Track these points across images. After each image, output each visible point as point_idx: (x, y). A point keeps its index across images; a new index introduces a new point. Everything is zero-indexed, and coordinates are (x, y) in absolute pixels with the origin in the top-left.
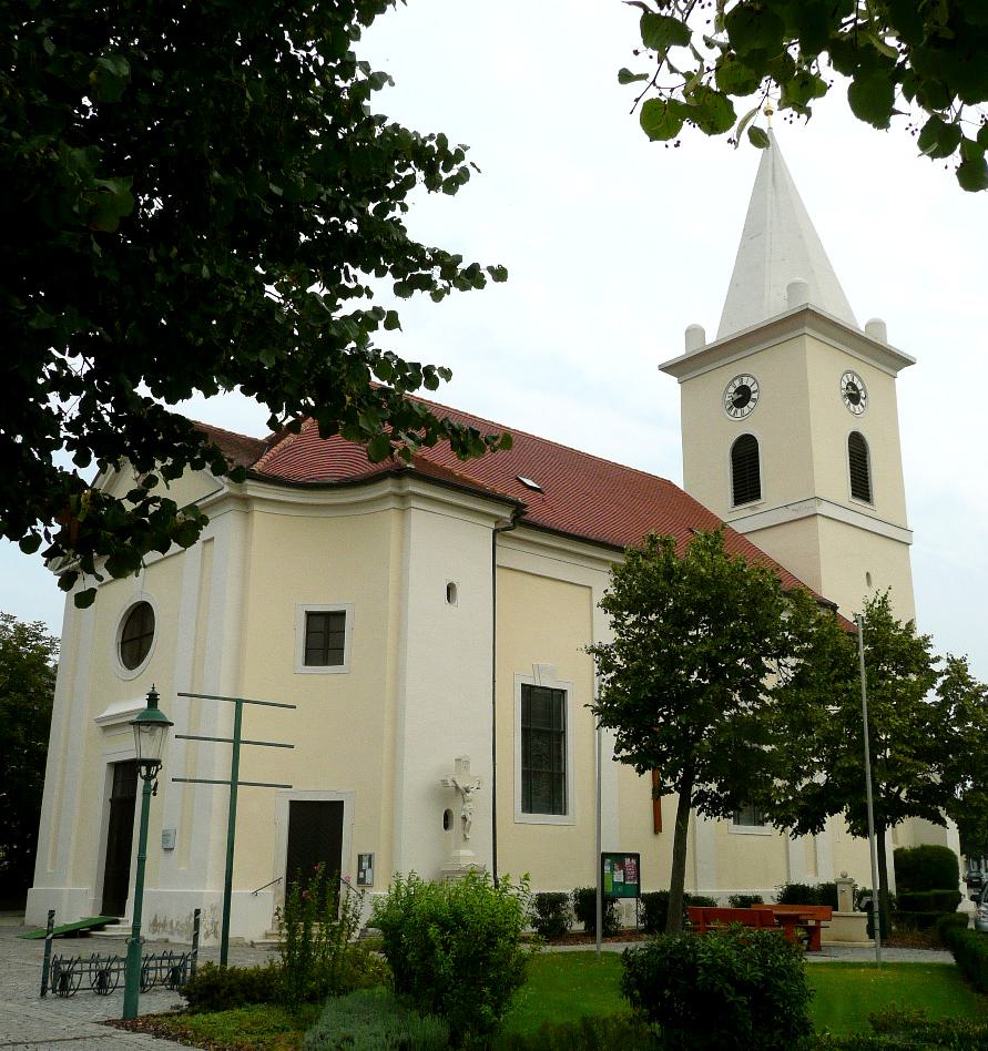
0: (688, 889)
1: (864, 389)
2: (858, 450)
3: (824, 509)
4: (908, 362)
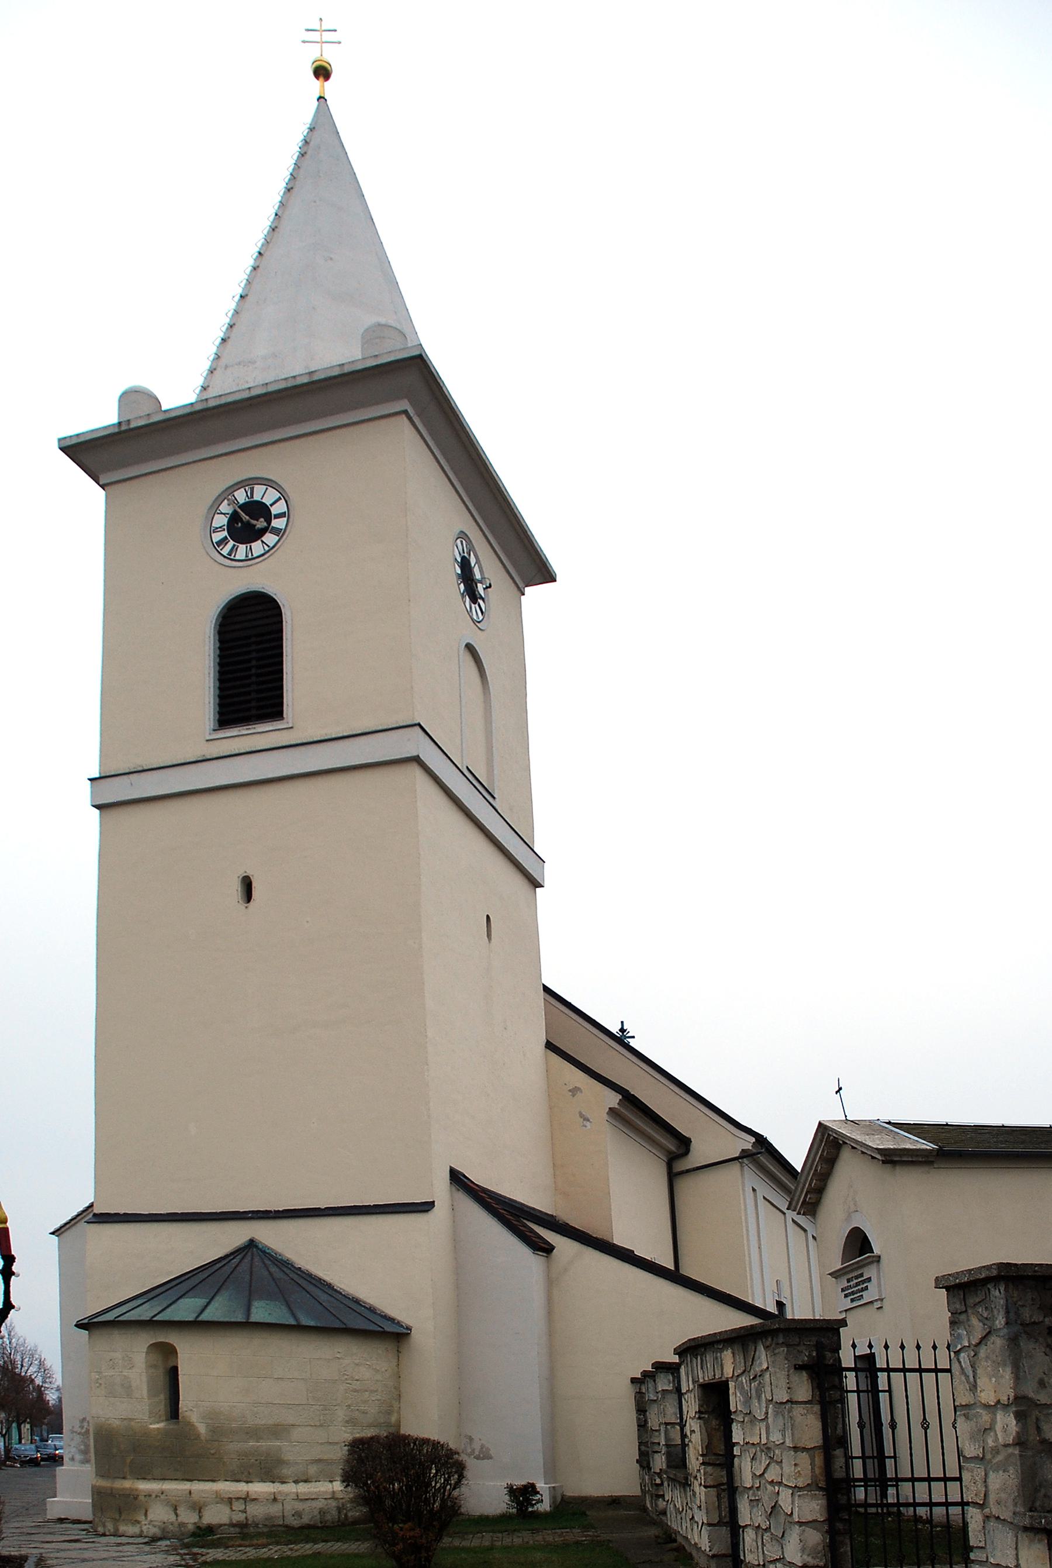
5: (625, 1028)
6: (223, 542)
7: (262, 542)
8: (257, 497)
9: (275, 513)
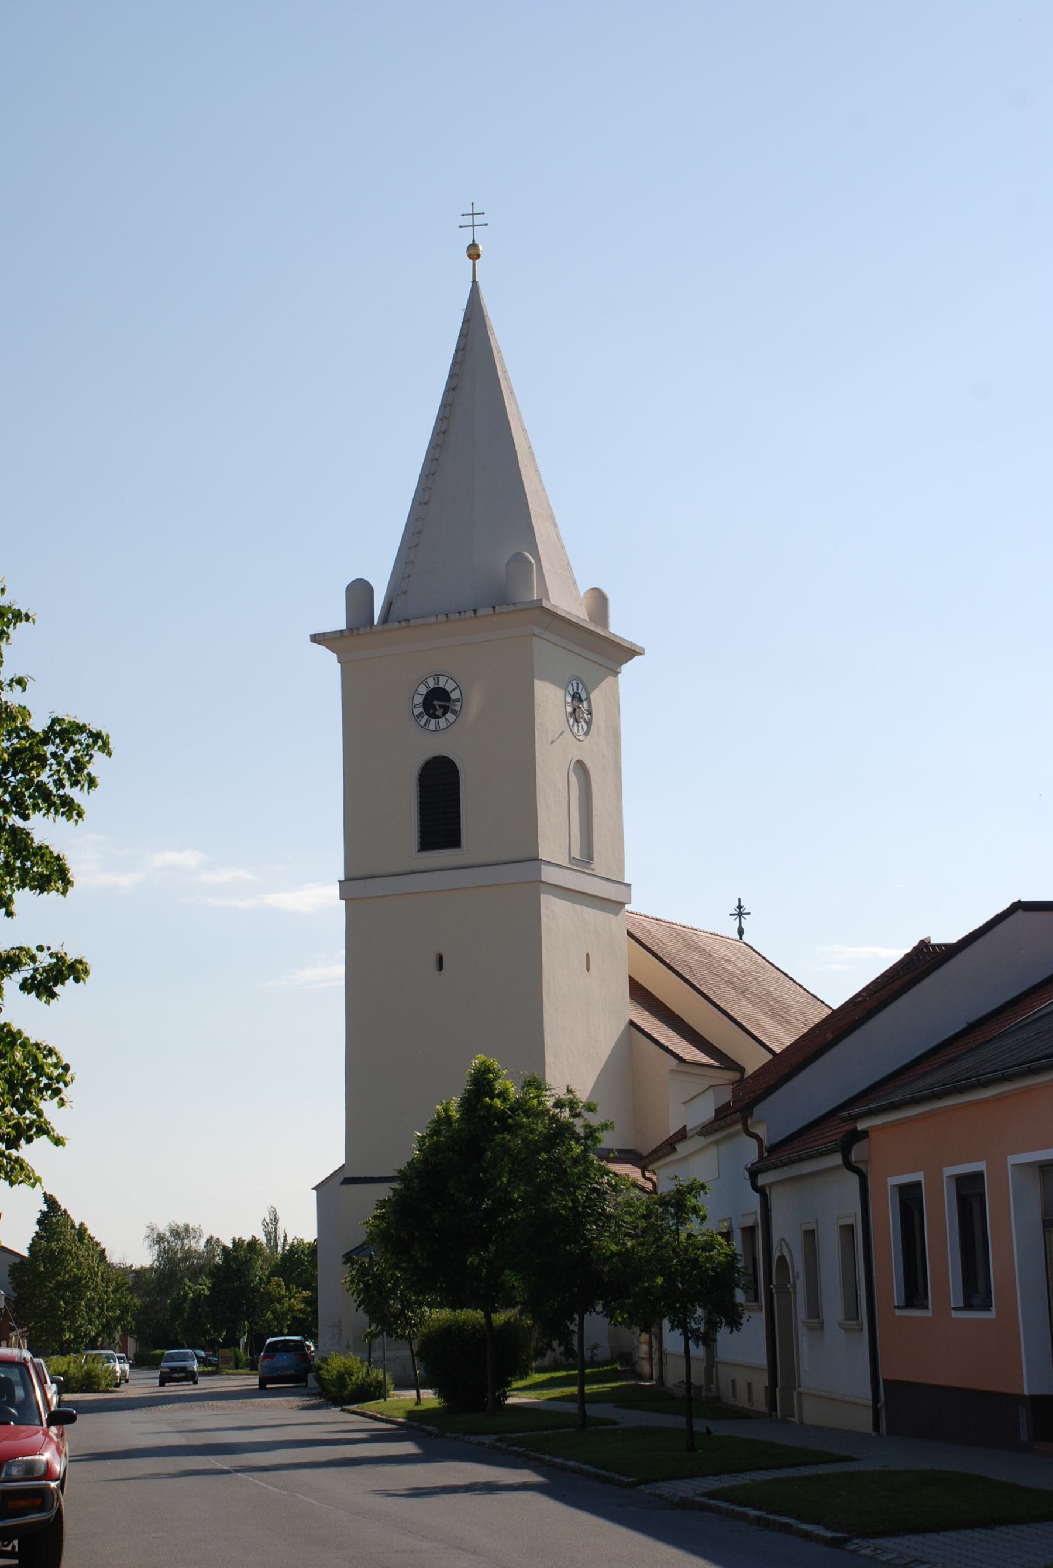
4: (629, 652)
5: (742, 905)
6: (420, 715)
7: (446, 719)
8: (441, 685)
9: (454, 698)
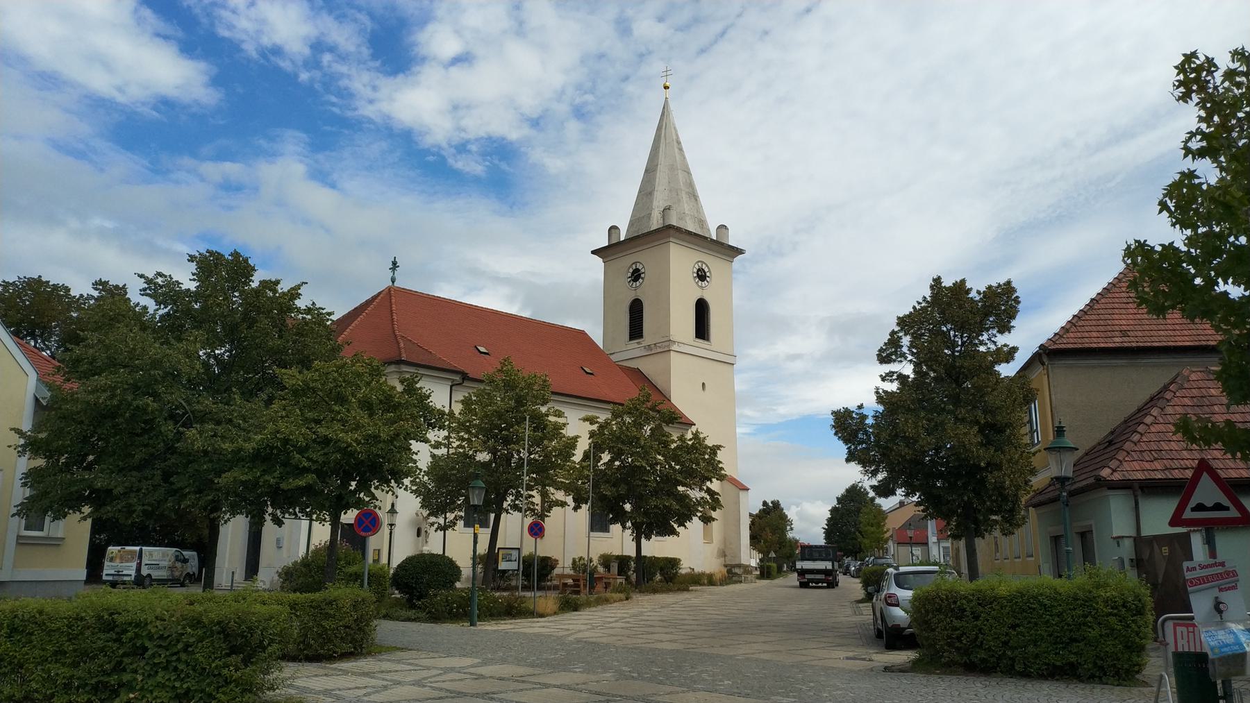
0: (446, 555)
1: (709, 271)
2: (702, 309)
3: (675, 347)
